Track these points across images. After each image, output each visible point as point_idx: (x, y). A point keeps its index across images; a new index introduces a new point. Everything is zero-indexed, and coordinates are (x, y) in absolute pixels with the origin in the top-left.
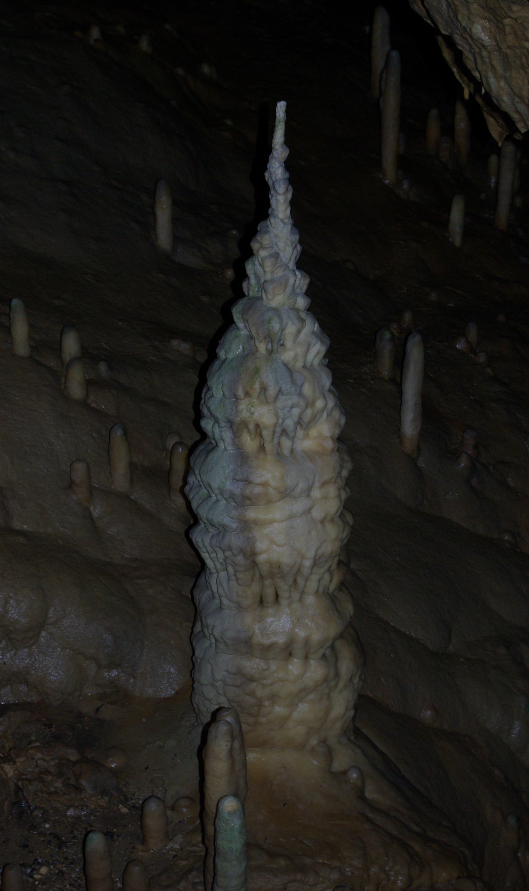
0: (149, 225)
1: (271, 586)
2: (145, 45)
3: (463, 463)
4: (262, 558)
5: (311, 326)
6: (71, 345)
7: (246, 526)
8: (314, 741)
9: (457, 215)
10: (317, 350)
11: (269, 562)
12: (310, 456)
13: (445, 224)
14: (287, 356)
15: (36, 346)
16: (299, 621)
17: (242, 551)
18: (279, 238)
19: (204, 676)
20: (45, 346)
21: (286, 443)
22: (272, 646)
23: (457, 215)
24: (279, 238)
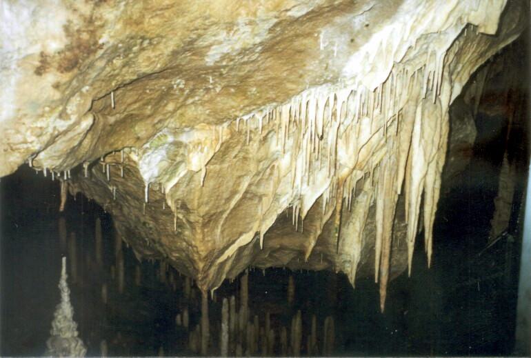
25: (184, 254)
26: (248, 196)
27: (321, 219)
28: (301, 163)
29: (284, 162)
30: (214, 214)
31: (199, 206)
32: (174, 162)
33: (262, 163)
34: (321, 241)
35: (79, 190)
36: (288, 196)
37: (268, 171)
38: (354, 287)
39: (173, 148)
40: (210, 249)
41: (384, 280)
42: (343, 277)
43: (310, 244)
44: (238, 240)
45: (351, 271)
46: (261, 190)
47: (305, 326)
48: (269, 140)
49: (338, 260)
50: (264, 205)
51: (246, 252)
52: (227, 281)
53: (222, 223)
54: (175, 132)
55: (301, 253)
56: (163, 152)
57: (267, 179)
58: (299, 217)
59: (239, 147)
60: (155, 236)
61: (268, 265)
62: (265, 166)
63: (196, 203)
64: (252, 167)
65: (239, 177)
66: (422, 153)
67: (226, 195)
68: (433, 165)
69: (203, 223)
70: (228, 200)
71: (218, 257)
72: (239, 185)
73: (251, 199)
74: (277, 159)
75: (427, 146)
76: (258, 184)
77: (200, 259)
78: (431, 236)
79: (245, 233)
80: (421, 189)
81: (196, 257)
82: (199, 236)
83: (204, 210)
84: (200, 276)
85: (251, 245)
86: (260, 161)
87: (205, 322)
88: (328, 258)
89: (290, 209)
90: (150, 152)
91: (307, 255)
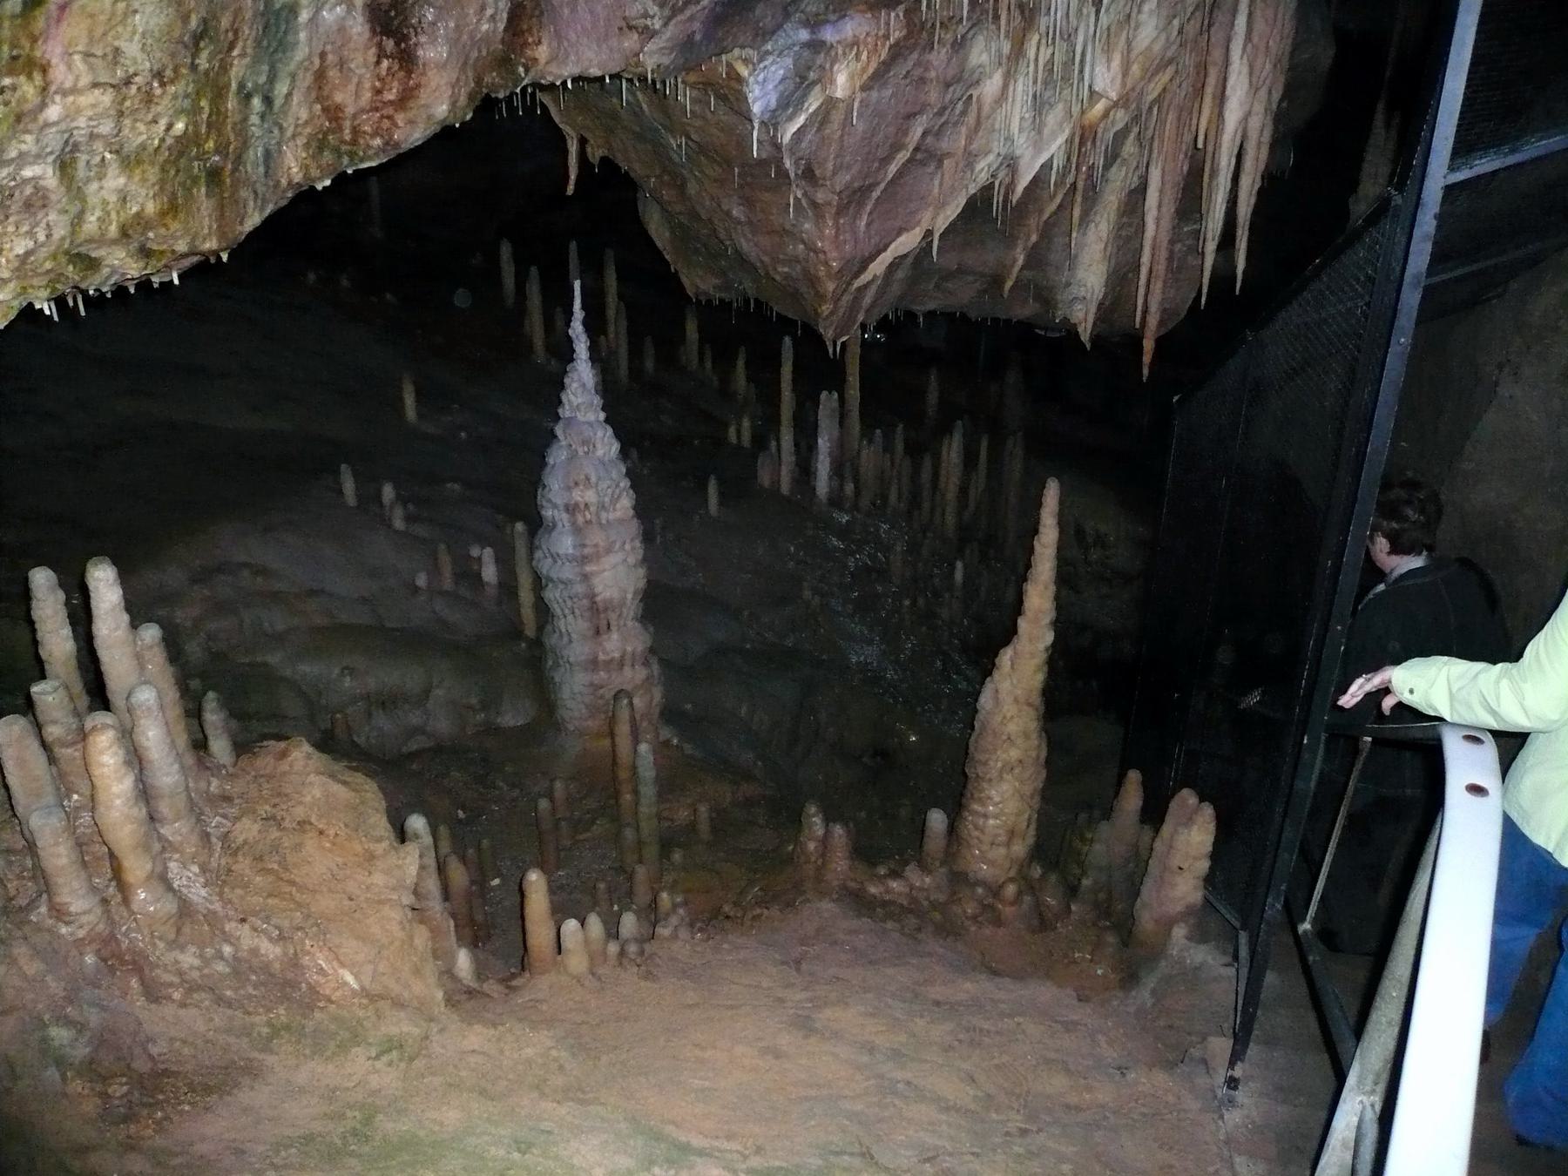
1: (599, 617)
4: (598, 599)
6: (388, 492)
7: (586, 577)
10: (616, 447)
11: (604, 601)
12: (621, 521)
14: (600, 453)
16: (626, 639)
18: (582, 377)
20: (369, 499)
22: (612, 660)
24: (582, 377)
25: (799, 268)
26: (919, 156)
27: (1041, 211)
28: (1022, 88)
29: (991, 87)
30: (860, 189)
31: (834, 173)
32: (801, 83)
34: (1036, 259)
37: (960, 106)
38: (1088, 346)
39: (806, 53)
41: (1153, 321)
42: (1072, 332)
43: (1015, 261)
44: (893, 246)
45: (1084, 318)
46: (944, 145)
47: (970, 459)
49: (1063, 297)
50: (947, 177)
51: (900, 274)
53: (868, 208)
54: (814, 24)
55: (997, 281)
56: (789, 61)
57: (956, 124)
58: (1006, 200)
59: (915, 55)
62: (958, 95)
63: (830, 166)
64: (933, 95)
66: (1245, 70)
67: (881, 153)
68: (1263, 93)
69: (838, 206)
70: (886, 161)
71: (857, 275)
72: (906, 133)
73: (923, 163)
74: (977, 82)
75: (1256, 56)
76: (938, 134)
77: (829, 276)
78: (1246, 233)
79: (907, 230)
80: (1238, 143)
83: (844, 178)
84: (826, 309)
85: (910, 260)
86: (948, 85)
87: (787, 437)
88: (1046, 299)
89: (988, 189)
90: (771, 59)
91: (1009, 284)
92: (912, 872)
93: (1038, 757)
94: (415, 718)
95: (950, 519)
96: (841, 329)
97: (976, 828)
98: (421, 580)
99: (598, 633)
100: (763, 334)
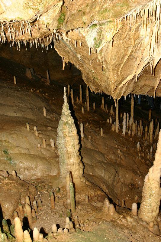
0: (42, 113)
2: (38, 91)
3: (90, 140)
5: (72, 118)
6: (35, 128)
8: (78, 177)
9: (83, 109)
13: (81, 111)
15: (30, 129)
17: (66, 150)
18: (66, 110)
19: (62, 170)
20: (32, 129)
21: (70, 135)
23: (83, 109)
30: (117, 65)
31: (111, 61)
33: (136, 41)
35: (69, 60)
36: (147, 57)
40: (116, 80)
43: (157, 83)
44: (128, 78)
46: (137, 55)
48: (140, 30)
52: (123, 97)
60: (95, 76)
61: (140, 93)
65: (127, 48)
67: (122, 56)
70: (123, 58)
79: (130, 75)
81: (111, 84)
82: (111, 74)
83: (113, 62)
92: (129, 219)
93: (159, 193)
94: (34, 172)
95: (151, 138)
96: (115, 97)
97: (144, 208)
98: (39, 146)
99: (69, 158)
100: (101, 99)
